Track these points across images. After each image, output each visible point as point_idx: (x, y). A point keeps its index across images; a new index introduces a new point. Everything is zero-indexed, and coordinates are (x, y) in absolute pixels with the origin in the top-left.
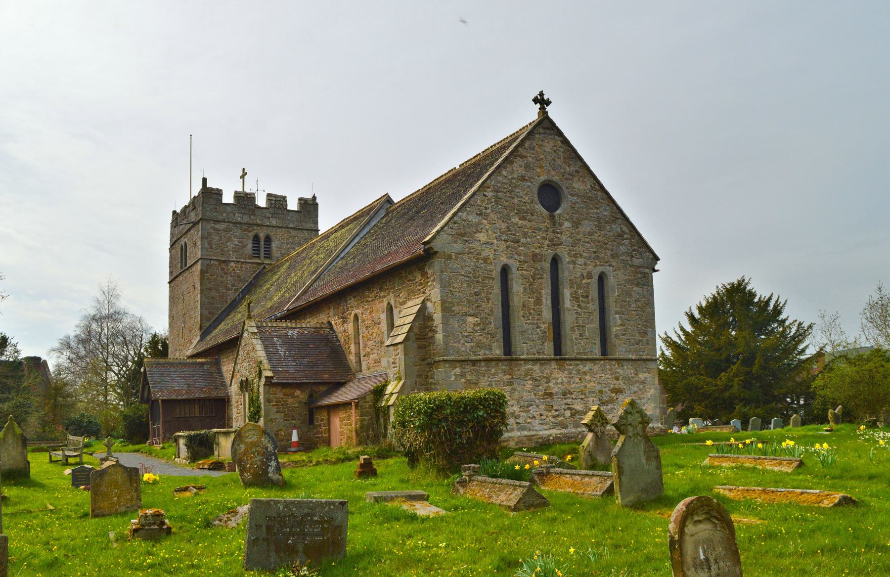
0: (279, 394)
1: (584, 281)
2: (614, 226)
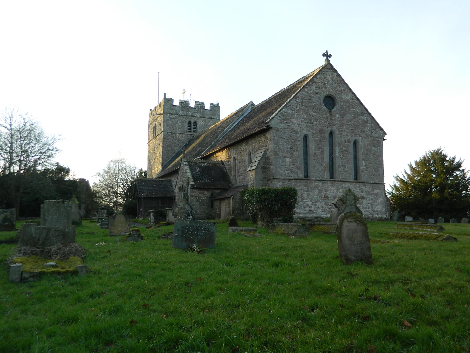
0: (197, 192)
1: (346, 144)
2: (362, 117)
